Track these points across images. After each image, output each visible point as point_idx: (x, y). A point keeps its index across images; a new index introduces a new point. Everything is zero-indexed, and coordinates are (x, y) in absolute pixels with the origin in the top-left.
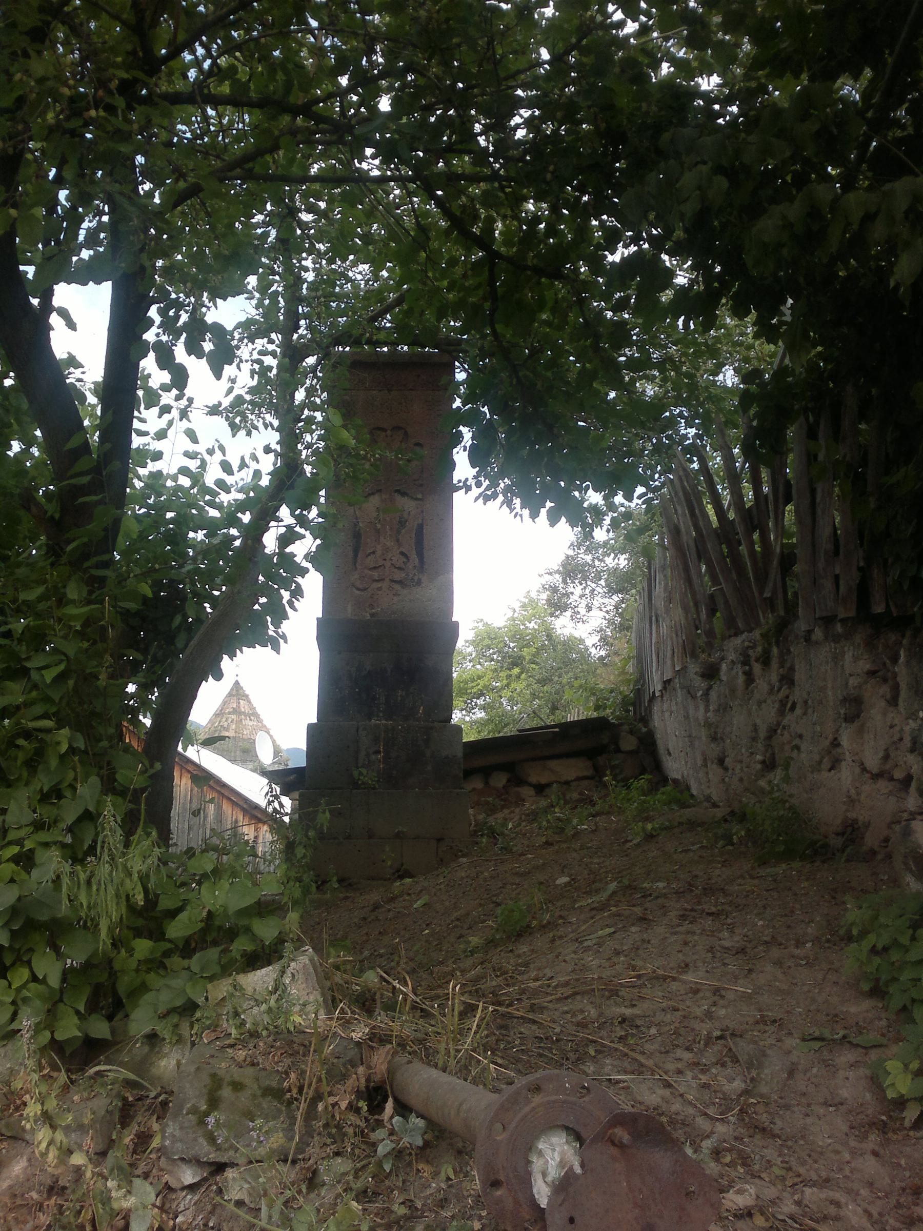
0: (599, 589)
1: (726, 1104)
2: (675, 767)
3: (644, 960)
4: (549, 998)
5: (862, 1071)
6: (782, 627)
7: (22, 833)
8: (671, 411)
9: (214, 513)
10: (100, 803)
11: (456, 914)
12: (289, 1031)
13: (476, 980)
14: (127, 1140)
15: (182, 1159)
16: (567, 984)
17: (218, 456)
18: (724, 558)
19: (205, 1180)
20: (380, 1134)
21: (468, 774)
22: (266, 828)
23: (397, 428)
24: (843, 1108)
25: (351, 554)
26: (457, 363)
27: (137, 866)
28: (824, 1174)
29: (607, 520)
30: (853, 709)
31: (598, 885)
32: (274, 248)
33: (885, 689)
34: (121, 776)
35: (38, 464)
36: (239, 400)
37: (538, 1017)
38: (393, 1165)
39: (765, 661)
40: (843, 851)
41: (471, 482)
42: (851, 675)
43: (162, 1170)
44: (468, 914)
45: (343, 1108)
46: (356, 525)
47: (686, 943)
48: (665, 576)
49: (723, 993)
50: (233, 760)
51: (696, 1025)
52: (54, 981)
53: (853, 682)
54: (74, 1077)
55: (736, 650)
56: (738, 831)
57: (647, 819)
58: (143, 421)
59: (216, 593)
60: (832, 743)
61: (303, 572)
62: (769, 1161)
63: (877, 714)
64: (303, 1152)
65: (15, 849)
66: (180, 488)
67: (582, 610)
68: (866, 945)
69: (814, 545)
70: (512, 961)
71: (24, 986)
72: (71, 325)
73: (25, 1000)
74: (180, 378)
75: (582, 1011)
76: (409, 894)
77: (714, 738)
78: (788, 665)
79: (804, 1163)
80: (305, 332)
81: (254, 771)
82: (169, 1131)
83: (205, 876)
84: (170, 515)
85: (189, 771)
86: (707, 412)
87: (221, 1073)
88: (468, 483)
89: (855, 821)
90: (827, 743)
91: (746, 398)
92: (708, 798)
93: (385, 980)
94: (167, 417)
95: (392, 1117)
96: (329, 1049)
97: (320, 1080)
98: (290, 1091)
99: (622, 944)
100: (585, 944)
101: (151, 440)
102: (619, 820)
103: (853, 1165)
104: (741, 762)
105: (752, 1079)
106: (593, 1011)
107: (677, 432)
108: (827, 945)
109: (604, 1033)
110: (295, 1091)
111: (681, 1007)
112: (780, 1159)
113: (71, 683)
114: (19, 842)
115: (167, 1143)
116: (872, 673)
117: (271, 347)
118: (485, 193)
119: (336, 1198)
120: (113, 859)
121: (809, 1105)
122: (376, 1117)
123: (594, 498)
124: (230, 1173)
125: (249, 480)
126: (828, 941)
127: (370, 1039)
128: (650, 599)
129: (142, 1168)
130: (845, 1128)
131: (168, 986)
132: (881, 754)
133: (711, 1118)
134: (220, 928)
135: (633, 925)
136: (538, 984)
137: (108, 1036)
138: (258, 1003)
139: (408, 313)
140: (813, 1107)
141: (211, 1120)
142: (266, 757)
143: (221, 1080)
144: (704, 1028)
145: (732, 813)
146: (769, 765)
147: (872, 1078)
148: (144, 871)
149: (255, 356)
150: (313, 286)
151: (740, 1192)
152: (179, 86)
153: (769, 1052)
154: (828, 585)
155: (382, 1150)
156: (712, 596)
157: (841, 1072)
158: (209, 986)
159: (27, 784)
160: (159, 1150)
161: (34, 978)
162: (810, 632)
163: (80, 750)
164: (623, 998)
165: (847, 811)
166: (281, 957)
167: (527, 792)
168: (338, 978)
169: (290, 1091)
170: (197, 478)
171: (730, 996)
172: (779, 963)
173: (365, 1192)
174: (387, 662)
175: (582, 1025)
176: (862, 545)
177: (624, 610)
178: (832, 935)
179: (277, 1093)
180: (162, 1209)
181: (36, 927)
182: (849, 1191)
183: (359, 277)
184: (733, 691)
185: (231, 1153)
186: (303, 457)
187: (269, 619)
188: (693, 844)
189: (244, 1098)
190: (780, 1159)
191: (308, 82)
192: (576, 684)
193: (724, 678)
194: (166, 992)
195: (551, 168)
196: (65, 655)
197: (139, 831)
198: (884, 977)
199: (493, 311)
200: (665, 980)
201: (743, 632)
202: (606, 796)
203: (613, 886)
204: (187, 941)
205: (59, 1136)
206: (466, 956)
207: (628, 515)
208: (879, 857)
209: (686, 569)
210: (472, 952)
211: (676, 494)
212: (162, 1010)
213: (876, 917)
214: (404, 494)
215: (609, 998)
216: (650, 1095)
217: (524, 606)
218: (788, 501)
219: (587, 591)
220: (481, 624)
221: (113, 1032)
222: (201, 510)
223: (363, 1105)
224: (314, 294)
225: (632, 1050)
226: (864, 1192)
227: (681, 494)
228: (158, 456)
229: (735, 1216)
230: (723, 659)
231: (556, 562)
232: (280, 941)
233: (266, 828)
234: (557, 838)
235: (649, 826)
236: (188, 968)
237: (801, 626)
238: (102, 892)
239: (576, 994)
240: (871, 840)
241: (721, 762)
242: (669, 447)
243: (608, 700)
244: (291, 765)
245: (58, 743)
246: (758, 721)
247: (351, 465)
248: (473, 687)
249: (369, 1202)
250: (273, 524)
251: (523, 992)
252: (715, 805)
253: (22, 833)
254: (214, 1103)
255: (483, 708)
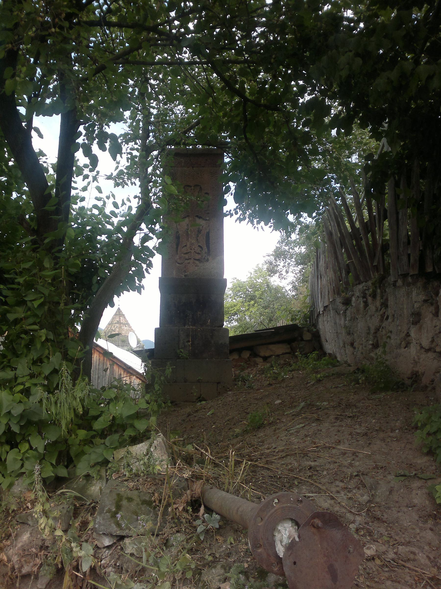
0: (292, 263)
1: (361, 507)
2: (329, 348)
3: (319, 439)
4: (275, 458)
5: (425, 491)
6: (382, 279)
7: (24, 379)
8: (328, 176)
9: (109, 227)
10: (61, 365)
11: (227, 418)
12: (154, 474)
13: (239, 450)
14: (77, 525)
15: (104, 534)
16: (283, 451)
17: (112, 199)
18: (354, 246)
19: (115, 543)
20: (198, 522)
21: (232, 351)
22: (134, 377)
23: (196, 186)
24: (415, 508)
25: (175, 247)
26: (225, 154)
27: (79, 395)
28: (407, 539)
29: (298, 230)
30: (417, 318)
31: (295, 404)
32: (138, 98)
33: (432, 309)
34: (71, 352)
35: (27, 203)
36: (121, 172)
37: (270, 466)
38: (205, 537)
39: (374, 296)
40: (412, 386)
41: (233, 212)
42: (415, 302)
43: (94, 539)
44: (233, 418)
45: (180, 510)
46: (177, 232)
47: (339, 431)
48: (325, 256)
49: (357, 454)
50: (118, 346)
51: (345, 470)
52: (41, 450)
53: (416, 305)
54: (51, 495)
55: (359, 291)
56: (362, 378)
57: (317, 372)
58: (75, 182)
59: (111, 265)
60: (406, 335)
61: (153, 255)
62: (381, 534)
63: (428, 321)
64: (162, 530)
65: (22, 387)
66: (93, 215)
67: (284, 273)
68: (425, 431)
69: (398, 240)
70: (256, 440)
71: (26, 452)
72: (41, 136)
73: (27, 458)
74: (94, 161)
75: (291, 464)
76: (205, 409)
77: (349, 334)
78: (385, 298)
79: (398, 534)
80: (152, 139)
81: (128, 350)
82: (97, 520)
83: (111, 400)
84: (88, 228)
85: (98, 351)
86: (345, 176)
87: (122, 493)
88: (231, 212)
89: (418, 372)
90: (404, 335)
91: (366, 169)
92: (346, 362)
93: (198, 450)
94: (87, 181)
95: (203, 514)
96: (174, 482)
97: (169, 497)
98: (155, 502)
99: (308, 432)
100: (291, 432)
101: (79, 191)
102: (303, 373)
103: (421, 535)
104: (362, 344)
105: (372, 495)
106: (296, 463)
107: (331, 186)
108: (406, 431)
109: (301, 474)
110: (157, 502)
111: (337, 461)
112: (387, 533)
113: (46, 307)
114: (22, 384)
115: (97, 526)
116: (425, 301)
117: (136, 146)
118: (241, 69)
119: (178, 553)
120: (67, 391)
121: (399, 507)
122: (196, 514)
123: (291, 218)
124: (127, 541)
125: (126, 211)
126: (406, 429)
127: (192, 477)
128: (317, 267)
129: (84, 538)
130: (417, 518)
131: (94, 452)
132: (430, 340)
133: (354, 514)
134: (118, 424)
135: (313, 422)
136: (269, 451)
137: (67, 476)
138: (138, 460)
139: (204, 128)
140: (401, 508)
141: (119, 516)
142: (133, 344)
143: (122, 496)
144: (349, 471)
145: (358, 369)
146: (376, 346)
147: (429, 494)
148: (82, 397)
149: (129, 151)
150: (157, 116)
151: (368, 548)
152: (92, 17)
153: (380, 482)
154: (405, 259)
155: (199, 530)
156: (348, 265)
157: (414, 491)
158: (115, 452)
159: (26, 356)
160: (92, 529)
161: (31, 448)
162: (396, 282)
163: (51, 340)
164: (310, 457)
165: (414, 367)
166: (150, 438)
167: (259, 360)
168: (176, 448)
169: (155, 502)
170: (101, 210)
171: (361, 456)
172: (383, 440)
173: (192, 549)
174: (193, 298)
175: (291, 470)
176: (421, 239)
177: (305, 273)
178: (408, 426)
179: (149, 503)
180: (94, 556)
181: (32, 424)
182: (420, 547)
183: (178, 112)
184: (358, 310)
185: (127, 531)
186: (152, 200)
187: (136, 278)
188: (340, 384)
189: (133, 506)
190: (387, 533)
191: (155, 15)
192: (283, 308)
193: (354, 304)
194: (94, 454)
195: (274, 56)
196: (43, 294)
197: (80, 378)
198: (434, 446)
199: (245, 127)
200: (329, 449)
201: (363, 282)
202: (297, 361)
203: (302, 404)
204: (103, 430)
205: (50, 521)
206: (234, 438)
207: (307, 227)
208: (429, 389)
209: (335, 253)
210: (237, 436)
211: (331, 216)
212: (92, 463)
213: (430, 417)
214: (200, 218)
215: (303, 457)
216: (324, 503)
217: (256, 271)
218: (385, 218)
219: (286, 264)
220: (235, 280)
221: (69, 473)
222: (103, 225)
223: (190, 508)
224: (157, 120)
225: (315, 482)
226: (427, 548)
227: (333, 216)
228: (83, 199)
229: (367, 560)
230: (353, 295)
231: (271, 249)
232: (148, 431)
233: (134, 377)
234: (274, 382)
235: (319, 376)
236: (104, 443)
237: (391, 279)
238: (62, 407)
239: (287, 455)
240: (425, 381)
241: (352, 344)
242: (327, 193)
243: (297, 316)
244: (146, 348)
245: (41, 337)
246: (370, 325)
247: (175, 204)
248: (231, 310)
249: (193, 554)
250: (138, 232)
251: (262, 454)
252: (349, 365)
253: (24, 379)
254: (119, 507)
255: (237, 320)
